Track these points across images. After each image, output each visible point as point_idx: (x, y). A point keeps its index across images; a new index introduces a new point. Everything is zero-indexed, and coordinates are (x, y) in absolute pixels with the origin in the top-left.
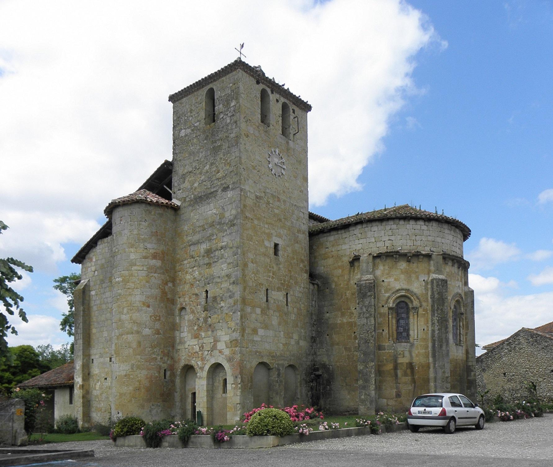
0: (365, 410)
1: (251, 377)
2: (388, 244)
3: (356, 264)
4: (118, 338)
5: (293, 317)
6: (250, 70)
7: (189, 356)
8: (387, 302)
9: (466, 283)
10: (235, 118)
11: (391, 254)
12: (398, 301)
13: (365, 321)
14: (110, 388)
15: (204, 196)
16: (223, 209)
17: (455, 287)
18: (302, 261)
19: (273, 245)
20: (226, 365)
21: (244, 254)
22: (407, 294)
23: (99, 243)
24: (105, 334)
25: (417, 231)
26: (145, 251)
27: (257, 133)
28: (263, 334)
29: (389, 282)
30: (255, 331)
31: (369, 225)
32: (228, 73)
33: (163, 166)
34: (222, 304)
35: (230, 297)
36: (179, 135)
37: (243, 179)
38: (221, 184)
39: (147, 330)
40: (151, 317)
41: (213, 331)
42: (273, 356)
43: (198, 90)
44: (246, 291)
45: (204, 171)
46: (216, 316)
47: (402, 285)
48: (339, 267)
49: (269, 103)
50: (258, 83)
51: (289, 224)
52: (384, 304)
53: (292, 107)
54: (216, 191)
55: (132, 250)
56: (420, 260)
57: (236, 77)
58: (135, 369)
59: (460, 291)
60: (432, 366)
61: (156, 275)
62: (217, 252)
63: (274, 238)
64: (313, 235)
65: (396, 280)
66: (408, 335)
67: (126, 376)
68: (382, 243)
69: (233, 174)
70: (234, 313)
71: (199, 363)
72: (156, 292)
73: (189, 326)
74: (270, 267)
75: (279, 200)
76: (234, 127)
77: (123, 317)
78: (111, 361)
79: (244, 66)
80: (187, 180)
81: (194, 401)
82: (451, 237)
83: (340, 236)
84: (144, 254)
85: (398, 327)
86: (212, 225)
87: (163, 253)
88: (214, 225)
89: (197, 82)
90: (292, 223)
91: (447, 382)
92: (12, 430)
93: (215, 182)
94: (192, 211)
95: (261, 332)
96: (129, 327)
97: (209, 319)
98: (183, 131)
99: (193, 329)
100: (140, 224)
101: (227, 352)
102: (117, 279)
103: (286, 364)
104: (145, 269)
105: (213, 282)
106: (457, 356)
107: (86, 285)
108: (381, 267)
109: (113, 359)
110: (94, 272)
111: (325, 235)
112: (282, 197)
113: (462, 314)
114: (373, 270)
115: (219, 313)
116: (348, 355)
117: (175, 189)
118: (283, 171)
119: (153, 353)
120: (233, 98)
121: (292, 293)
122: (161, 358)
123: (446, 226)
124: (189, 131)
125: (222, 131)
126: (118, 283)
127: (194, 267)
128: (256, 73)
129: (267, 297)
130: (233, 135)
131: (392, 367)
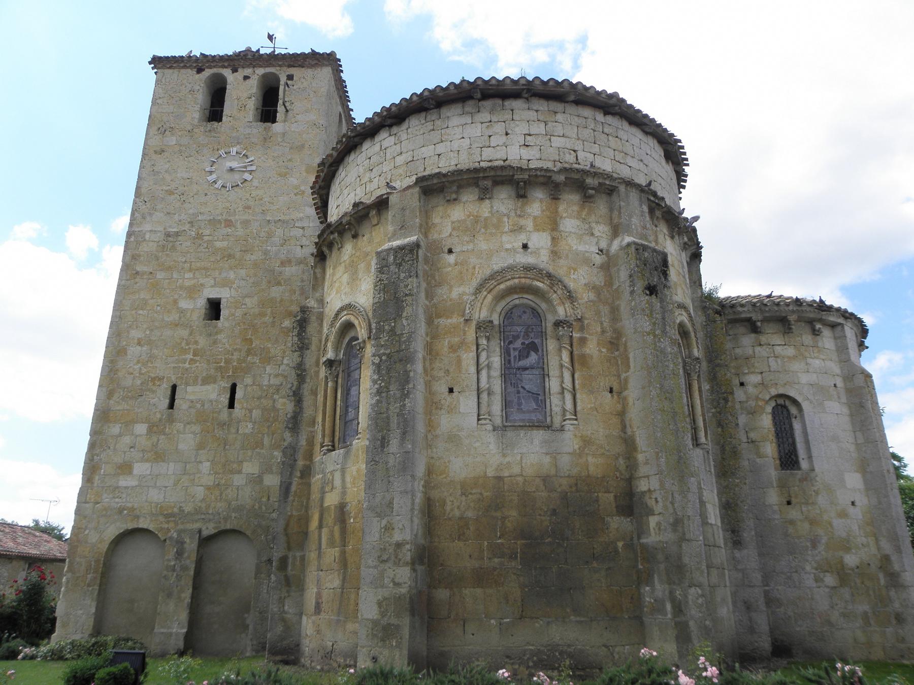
91: (397, 563)
95: (140, 468)
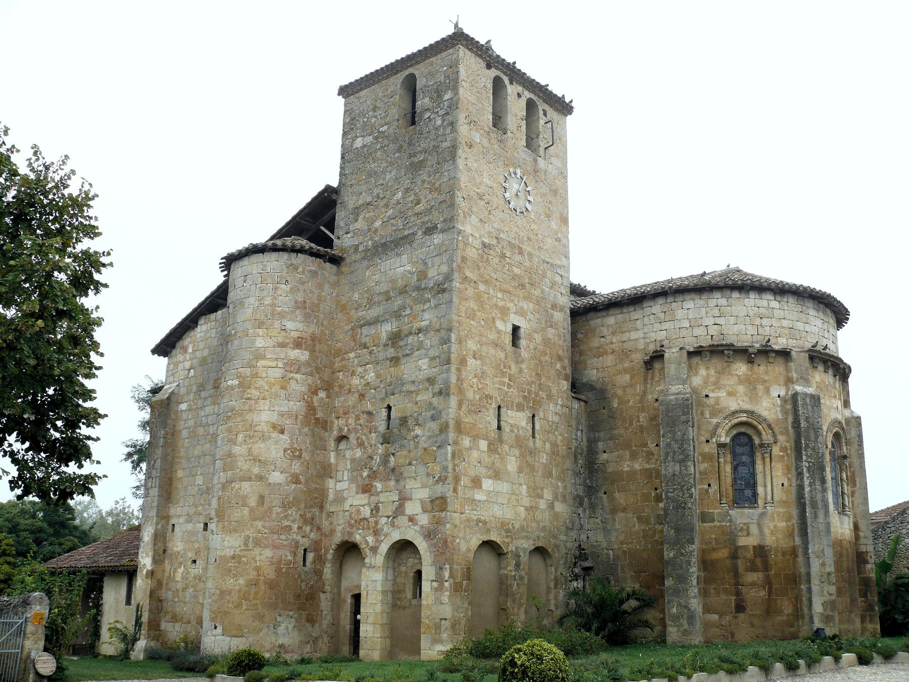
0: (680, 634)
1: (468, 569)
2: (713, 330)
3: (657, 365)
4: (224, 488)
5: (544, 458)
6: (477, 47)
7: (351, 526)
8: (714, 433)
9: (846, 404)
10: (450, 118)
11: (720, 348)
12: (735, 432)
13: (677, 468)
14: (199, 578)
15: (392, 242)
16: (425, 264)
17: (831, 410)
18: (560, 359)
19: (510, 329)
20: (422, 545)
21: (460, 343)
22: (750, 420)
23: (202, 321)
24: (199, 480)
25: (762, 311)
26: (283, 333)
27: (485, 142)
28: (492, 489)
29: (718, 399)
30: (477, 483)
31: (680, 298)
32: (441, 51)
33: (321, 194)
34: (418, 431)
35: (433, 418)
36: (352, 146)
37: (462, 215)
38: (423, 223)
39: (277, 474)
40: (285, 450)
41: (397, 481)
42: (508, 531)
43: (387, 77)
44: (463, 409)
45: (392, 202)
46: (405, 452)
47: (741, 403)
48: (626, 371)
49: (506, 99)
50: (489, 67)
51: (536, 293)
52: (709, 438)
53: (542, 106)
54: (414, 234)
55: (260, 332)
56: (771, 360)
57: (455, 56)
58: (250, 546)
59: (839, 417)
60: (800, 552)
61: (298, 376)
62: (411, 337)
63: (512, 316)
64: (576, 314)
65: (730, 394)
66: (755, 495)
67: (233, 557)
68: (703, 329)
69: (444, 206)
70: (439, 447)
71: (370, 539)
72: (297, 406)
73: (352, 470)
74: (505, 367)
75: (521, 253)
76: (448, 131)
77: (236, 450)
78: (205, 529)
79: (467, 40)
80: (361, 217)
81: (357, 609)
82: (819, 323)
83: (626, 316)
84: (280, 340)
85: (735, 480)
86: (403, 291)
87: (313, 338)
88: (406, 292)
89: (387, 66)
90: (543, 292)
91: (829, 583)
92: (22, 651)
93: (412, 219)
94: (368, 268)
95: (487, 484)
96: (245, 467)
97: (392, 459)
98: (360, 139)
99: (361, 476)
100: (276, 288)
101: (424, 520)
102: (230, 383)
103: (529, 545)
104: (280, 365)
105: (401, 392)
106: (842, 534)
107: (172, 393)
108: (703, 372)
109: (212, 526)
110: (189, 370)
111: (599, 314)
112: (527, 248)
113: (845, 457)
114: (689, 377)
115: (412, 447)
116: (644, 530)
117: (339, 232)
118: (528, 205)
119: (286, 517)
120: (448, 88)
121: (541, 414)
122: (299, 528)
123: (810, 304)
124: (369, 139)
125: (427, 138)
126: (232, 388)
127: (368, 363)
128: (486, 53)
129: (499, 421)
130: (445, 145)
131: (726, 555)
